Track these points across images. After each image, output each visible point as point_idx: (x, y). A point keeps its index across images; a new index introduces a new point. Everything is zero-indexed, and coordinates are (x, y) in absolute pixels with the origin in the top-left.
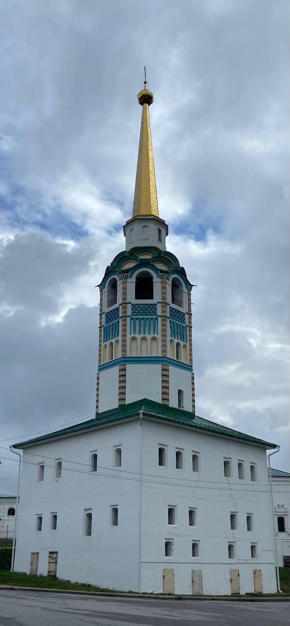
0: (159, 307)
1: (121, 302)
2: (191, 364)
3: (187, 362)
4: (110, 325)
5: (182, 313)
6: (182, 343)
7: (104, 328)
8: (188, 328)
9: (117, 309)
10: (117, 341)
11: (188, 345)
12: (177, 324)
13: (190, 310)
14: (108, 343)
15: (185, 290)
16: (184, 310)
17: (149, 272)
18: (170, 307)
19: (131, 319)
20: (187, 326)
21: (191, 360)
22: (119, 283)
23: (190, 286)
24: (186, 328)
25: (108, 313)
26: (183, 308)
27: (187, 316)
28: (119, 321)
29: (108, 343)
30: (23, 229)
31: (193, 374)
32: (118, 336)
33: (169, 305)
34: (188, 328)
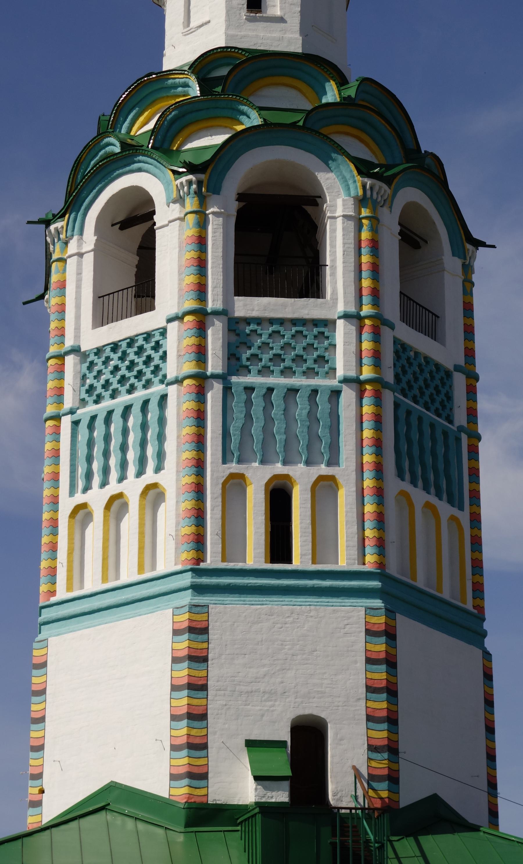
0: (342, 333)
1: (174, 310)
2: (481, 609)
3: (465, 602)
4: (127, 409)
5: (438, 366)
6: (302, 478)
7: (76, 423)
8: (464, 438)
9: (154, 339)
10: (153, 494)
11: (464, 517)
12: (432, 426)
13: (470, 354)
14: (97, 498)
15: (452, 264)
16: (445, 353)
17: (426, 210)
18: (396, 341)
19: (227, 390)
20: (461, 429)
21: (478, 589)
22: (165, 214)
23: (466, 242)
24: (458, 440)
25: (99, 351)
26: (443, 343)
27: (459, 382)
28: (164, 398)
29: (97, 498)
30: (174, 92)
31: (487, 656)
32: (158, 469)
33: (392, 327)
34: (464, 438)
